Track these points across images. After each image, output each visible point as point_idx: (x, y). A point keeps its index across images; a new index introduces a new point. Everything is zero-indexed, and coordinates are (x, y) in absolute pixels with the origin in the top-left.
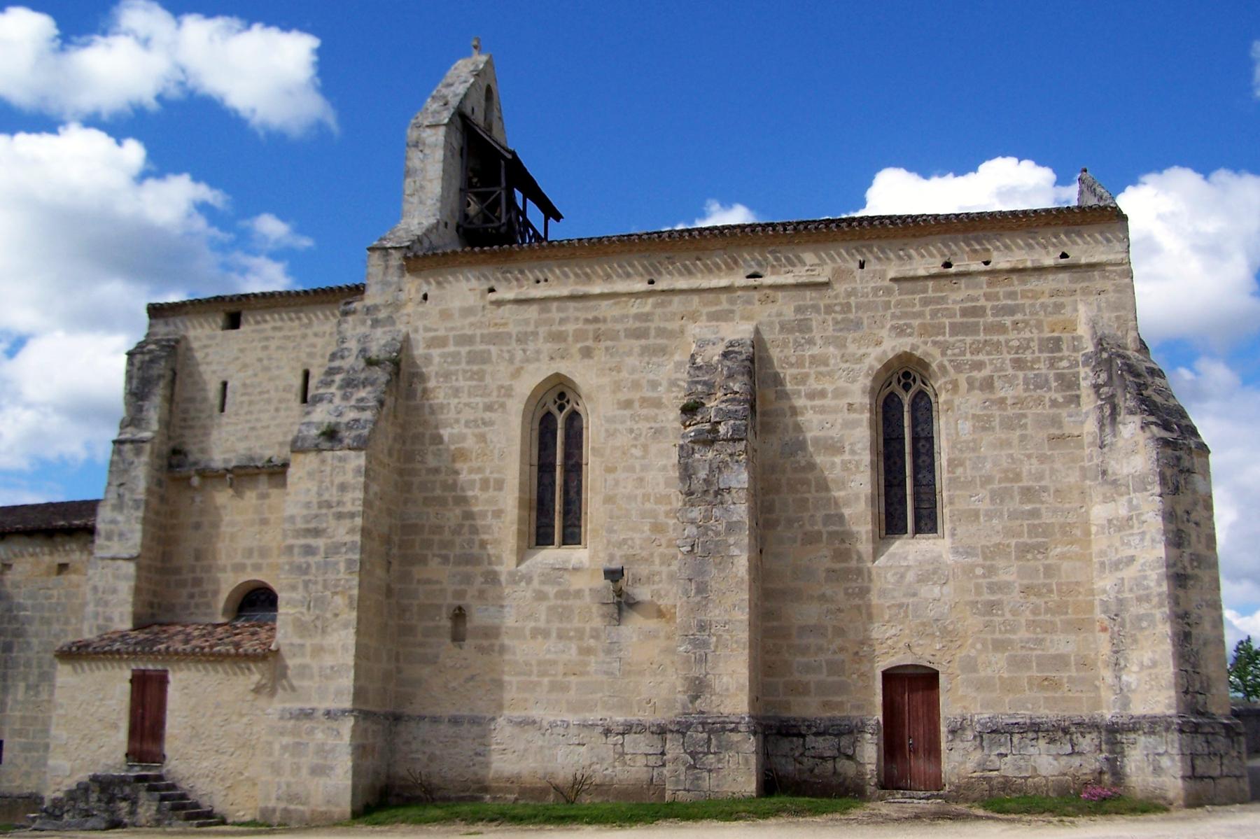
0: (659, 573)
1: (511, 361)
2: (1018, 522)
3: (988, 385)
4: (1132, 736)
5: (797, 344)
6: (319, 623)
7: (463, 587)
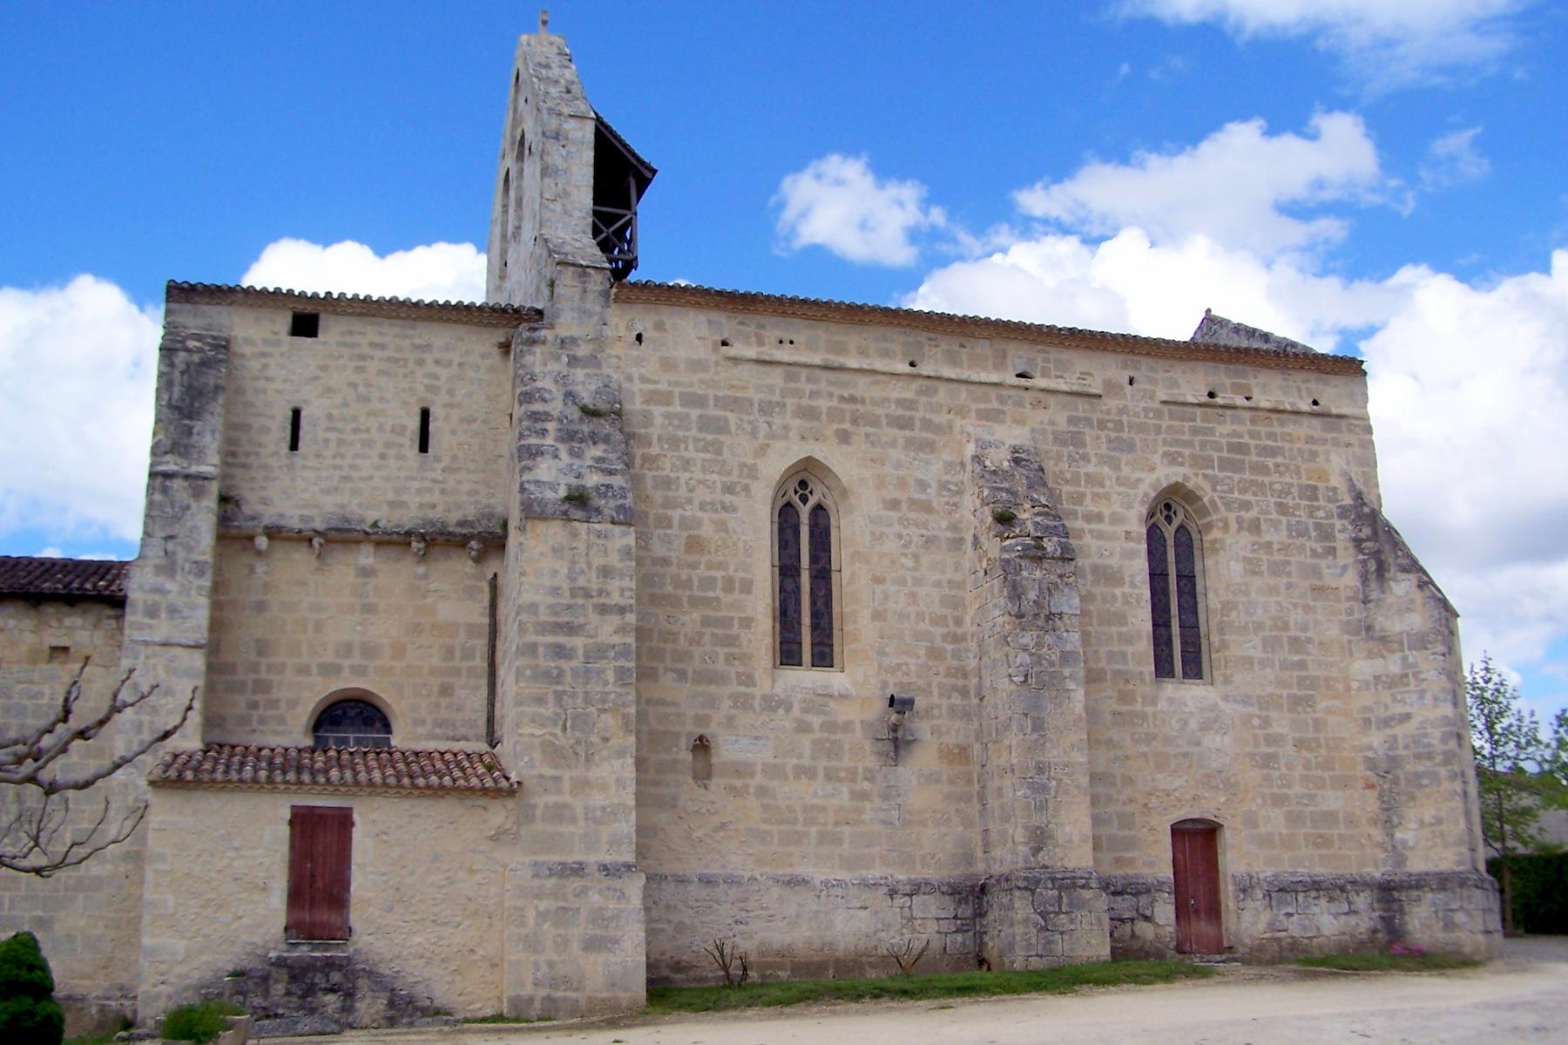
0: (939, 706)
1: (754, 434)
2: (1288, 673)
3: (1255, 527)
4: (1415, 893)
5: (1072, 460)
6: (581, 750)
7: (707, 711)
